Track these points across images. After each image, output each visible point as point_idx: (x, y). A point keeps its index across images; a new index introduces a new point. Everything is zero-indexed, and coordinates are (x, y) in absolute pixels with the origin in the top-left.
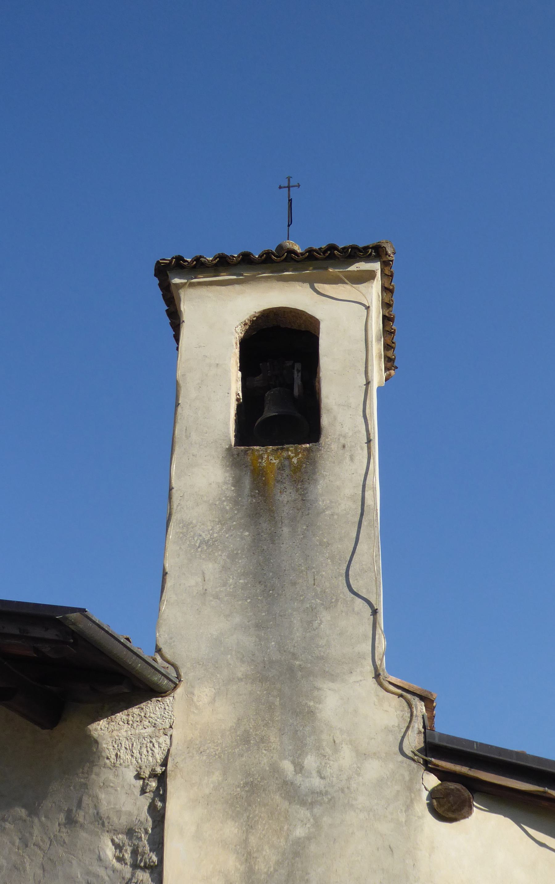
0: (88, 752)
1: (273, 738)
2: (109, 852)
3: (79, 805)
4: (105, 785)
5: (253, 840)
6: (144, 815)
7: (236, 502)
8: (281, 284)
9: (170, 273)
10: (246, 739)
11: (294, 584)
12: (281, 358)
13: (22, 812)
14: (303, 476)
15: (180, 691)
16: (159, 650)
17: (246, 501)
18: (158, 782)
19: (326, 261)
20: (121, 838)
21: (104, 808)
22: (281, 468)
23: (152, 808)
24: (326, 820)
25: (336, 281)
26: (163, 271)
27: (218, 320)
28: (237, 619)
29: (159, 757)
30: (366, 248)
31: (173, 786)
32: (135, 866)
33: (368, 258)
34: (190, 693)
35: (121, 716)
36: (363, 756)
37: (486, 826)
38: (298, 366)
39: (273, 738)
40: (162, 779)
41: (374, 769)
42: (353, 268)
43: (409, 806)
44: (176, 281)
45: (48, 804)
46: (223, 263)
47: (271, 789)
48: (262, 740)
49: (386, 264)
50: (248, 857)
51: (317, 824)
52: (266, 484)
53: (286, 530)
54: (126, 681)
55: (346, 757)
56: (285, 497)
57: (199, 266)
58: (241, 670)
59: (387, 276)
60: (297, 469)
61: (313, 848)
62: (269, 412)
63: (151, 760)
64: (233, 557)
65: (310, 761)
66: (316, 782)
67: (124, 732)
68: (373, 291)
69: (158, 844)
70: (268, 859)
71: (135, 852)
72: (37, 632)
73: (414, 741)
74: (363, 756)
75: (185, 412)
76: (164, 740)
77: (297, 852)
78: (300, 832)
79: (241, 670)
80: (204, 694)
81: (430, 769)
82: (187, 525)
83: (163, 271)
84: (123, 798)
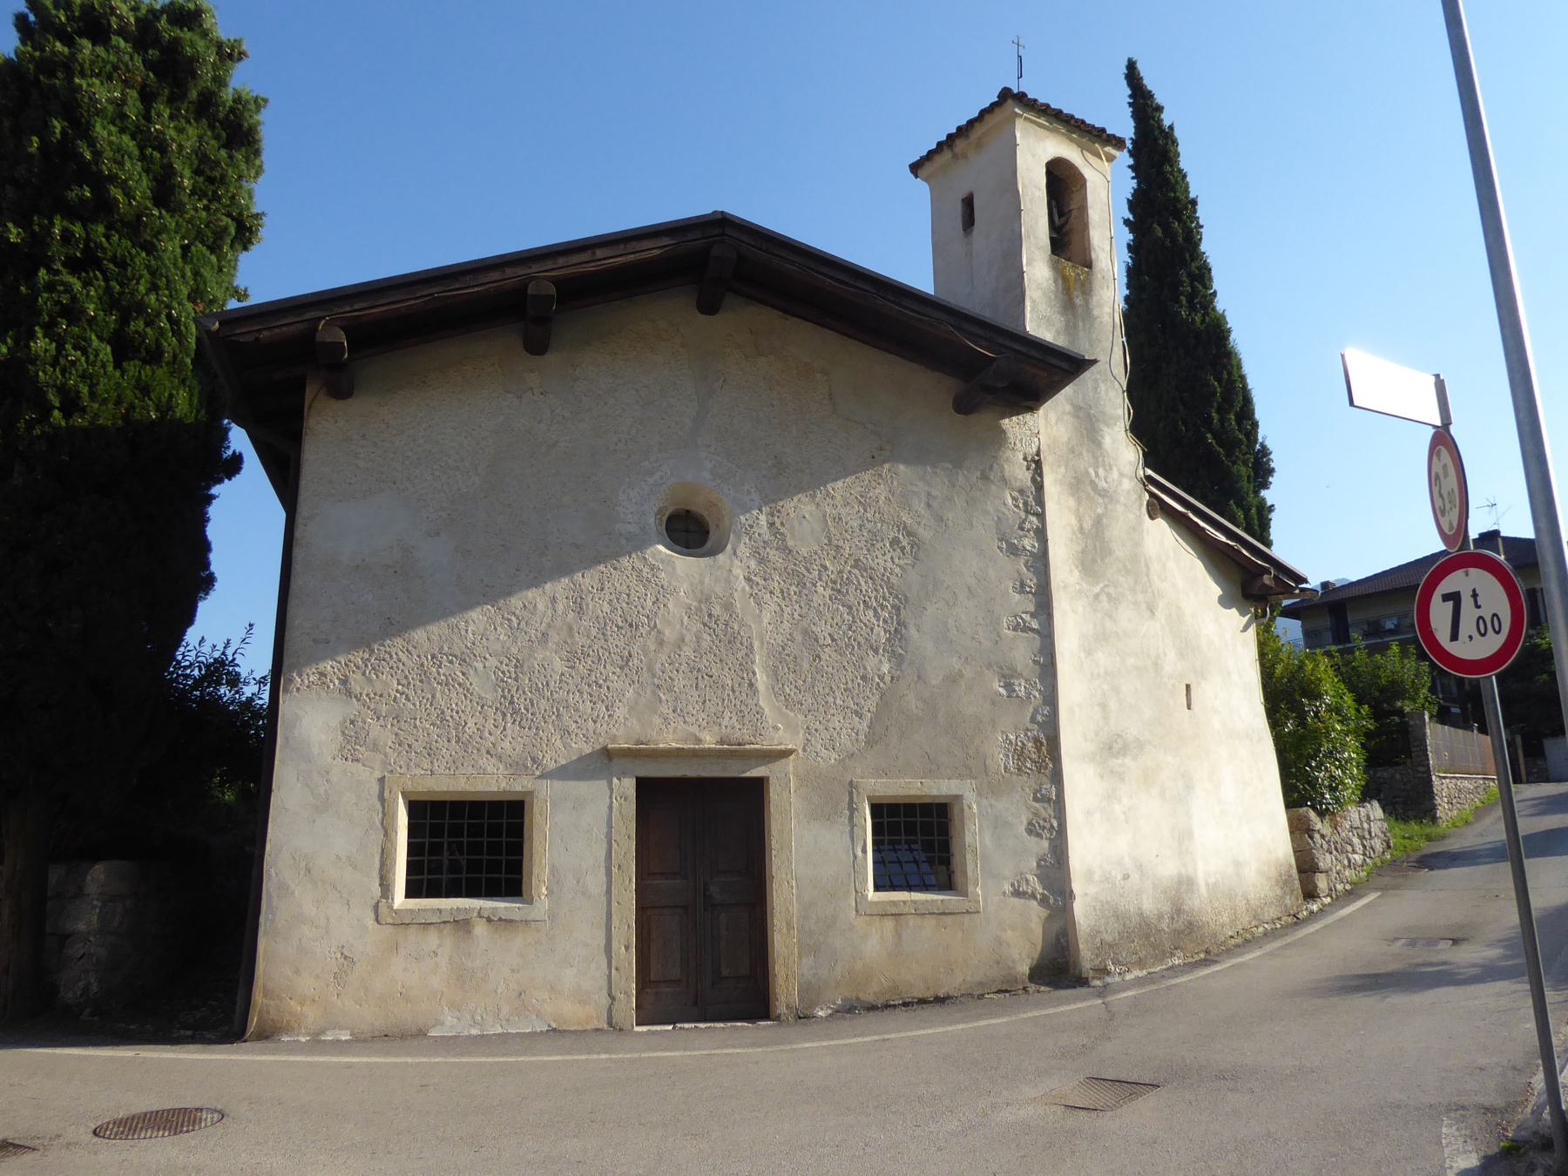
0: (1000, 437)
3: (991, 468)
4: (1007, 460)
18: (1036, 465)
20: (1015, 494)
23: (1033, 480)
31: (1046, 469)
32: (1027, 512)
36: (1122, 475)
37: (1161, 524)
40: (1038, 464)
50: (1080, 519)
69: (1040, 501)
70: (1088, 524)
71: (1025, 504)
78: (1099, 511)
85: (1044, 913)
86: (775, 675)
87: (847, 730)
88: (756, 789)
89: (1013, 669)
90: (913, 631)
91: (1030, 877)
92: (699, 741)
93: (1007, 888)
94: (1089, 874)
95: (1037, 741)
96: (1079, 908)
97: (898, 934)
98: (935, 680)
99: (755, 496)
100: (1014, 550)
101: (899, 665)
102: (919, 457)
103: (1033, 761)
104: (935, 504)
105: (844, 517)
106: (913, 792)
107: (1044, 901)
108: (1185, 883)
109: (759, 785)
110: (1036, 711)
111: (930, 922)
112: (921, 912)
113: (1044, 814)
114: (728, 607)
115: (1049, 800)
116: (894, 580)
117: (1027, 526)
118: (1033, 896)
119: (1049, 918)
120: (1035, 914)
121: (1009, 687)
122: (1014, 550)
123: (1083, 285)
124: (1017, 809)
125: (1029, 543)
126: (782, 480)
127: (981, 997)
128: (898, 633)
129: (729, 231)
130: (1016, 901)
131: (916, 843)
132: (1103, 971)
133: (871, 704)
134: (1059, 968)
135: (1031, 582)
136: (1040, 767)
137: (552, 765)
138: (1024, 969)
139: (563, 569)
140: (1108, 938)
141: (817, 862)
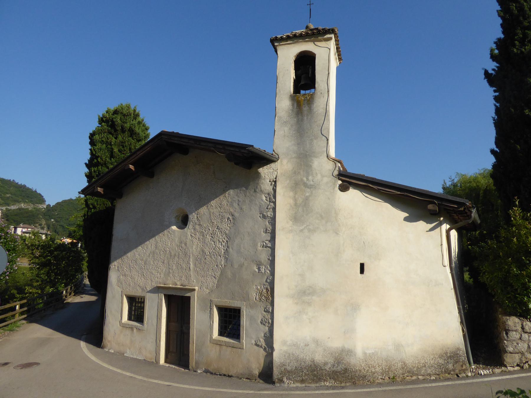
0: (258, 176)
1: (302, 172)
2: (264, 198)
4: (262, 183)
5: (297, 196)
6: (272, 190)
7: (293, 111)
8: (305, 43)
9: (275, 41)
10: (295, 173)
11: (307, 133)
12: (305, 65)
13: (244, 189)
14: (310, 101)
15: (279, 161)
16: (274, 151)
17: (295, 110)
19: (316, 34)
20: (267, 195)
21: (262, 189)
22: (304, 100)
23: (273, 189)
24: (314, 192)
25: (320, 41)
26: (273, 41)
27: (288, 54)
28: (293, 142)
29: (275, 177)
30: (329, 30)
32: (270, 202)
33: (330, 33)
34: (281, 162)
35: (265, 167)
36: (323, 176)
37: (353, 193)
38: (311, 67)
39: (302, 172)
40: (275, 182)
41: (326, 180)
42: (326, 37)
43: (334, 189)
44: (276, 44)
45: (250, 187)
46: (288, 38)
47: (301, 184)
48: (299, 173)
49: (335, 34)
50: (295, 200)
51: (312, 193)
52: (300, 105)
53: (305, 118)
54: (266, 160)
55: (319, 177)
56: (305, 109)
57: (282, 39)
58: (294, 156)
59: (336, 37)
60: (309, 100)
61: (310, 198)
62: (302, 83)
63: (273, 177)
64: (292, 126)
65: (310, 178)
66: (312, 183)
67: (266, 171)
68: (332, 44)
69: (275, 197)
70: (300, 201)
71: (270, 199)
72: (243, 151)
73: (336, 173)
74: (323, 176)
75: (279, 85)
76: (276, 173)
77: (307, 199)
78: (307, 194)
79: (294, 156)
80: (285, 161)
81: (339, 179)
82: (280, 117)
83: (273, 41)
84: (267, 186)
85: (265, 354)
86: (195, 265)
87: (212, 282)
88: (187, 300)
89: (260, 262)
90: (231, 249)
91: (261, 340)
92: (176, 285)
93: (253, 342)
94: (284, 343)
95: (267, 289)
96: (275, 354)
97: (220, 351)
98: (236, 266)
99: (194, 209)
100: (264, 217)
101: (226, 261)
102: (237, 186)
103: (265, 297)
104: (240, 204)
105: (216, 211)
106: (227, 305)
107: (265, 349)
108: (350, 352)
109: (189, 298)
110: (267, 278)
111: (229, 349)
112: (227, 345)
113: (267, 317)
114: (186, 244)
115: (269, 312)
116: (227, 232)
117: (269, 207)
118: (261, 347)
119: (266, 356)
120: (262, 353)
121: (259, 269)
122: (264, 217)
123: (309, 100)
124: (259, 314)
125: (270, 214)
126: (202, 201)
127: (241, 379)
128: (226, 251)
129: (163, 136)
130: (256, 347)
131: (230, 322)
132: (281, 381)
133: (218, 274)
134: (267, 375)
135: (270, 228)
136: (267, 299)
137: (149, 289)
138: (257, 372)
139: (154, 236)
140: (289, 368)
141: (205, 324)
